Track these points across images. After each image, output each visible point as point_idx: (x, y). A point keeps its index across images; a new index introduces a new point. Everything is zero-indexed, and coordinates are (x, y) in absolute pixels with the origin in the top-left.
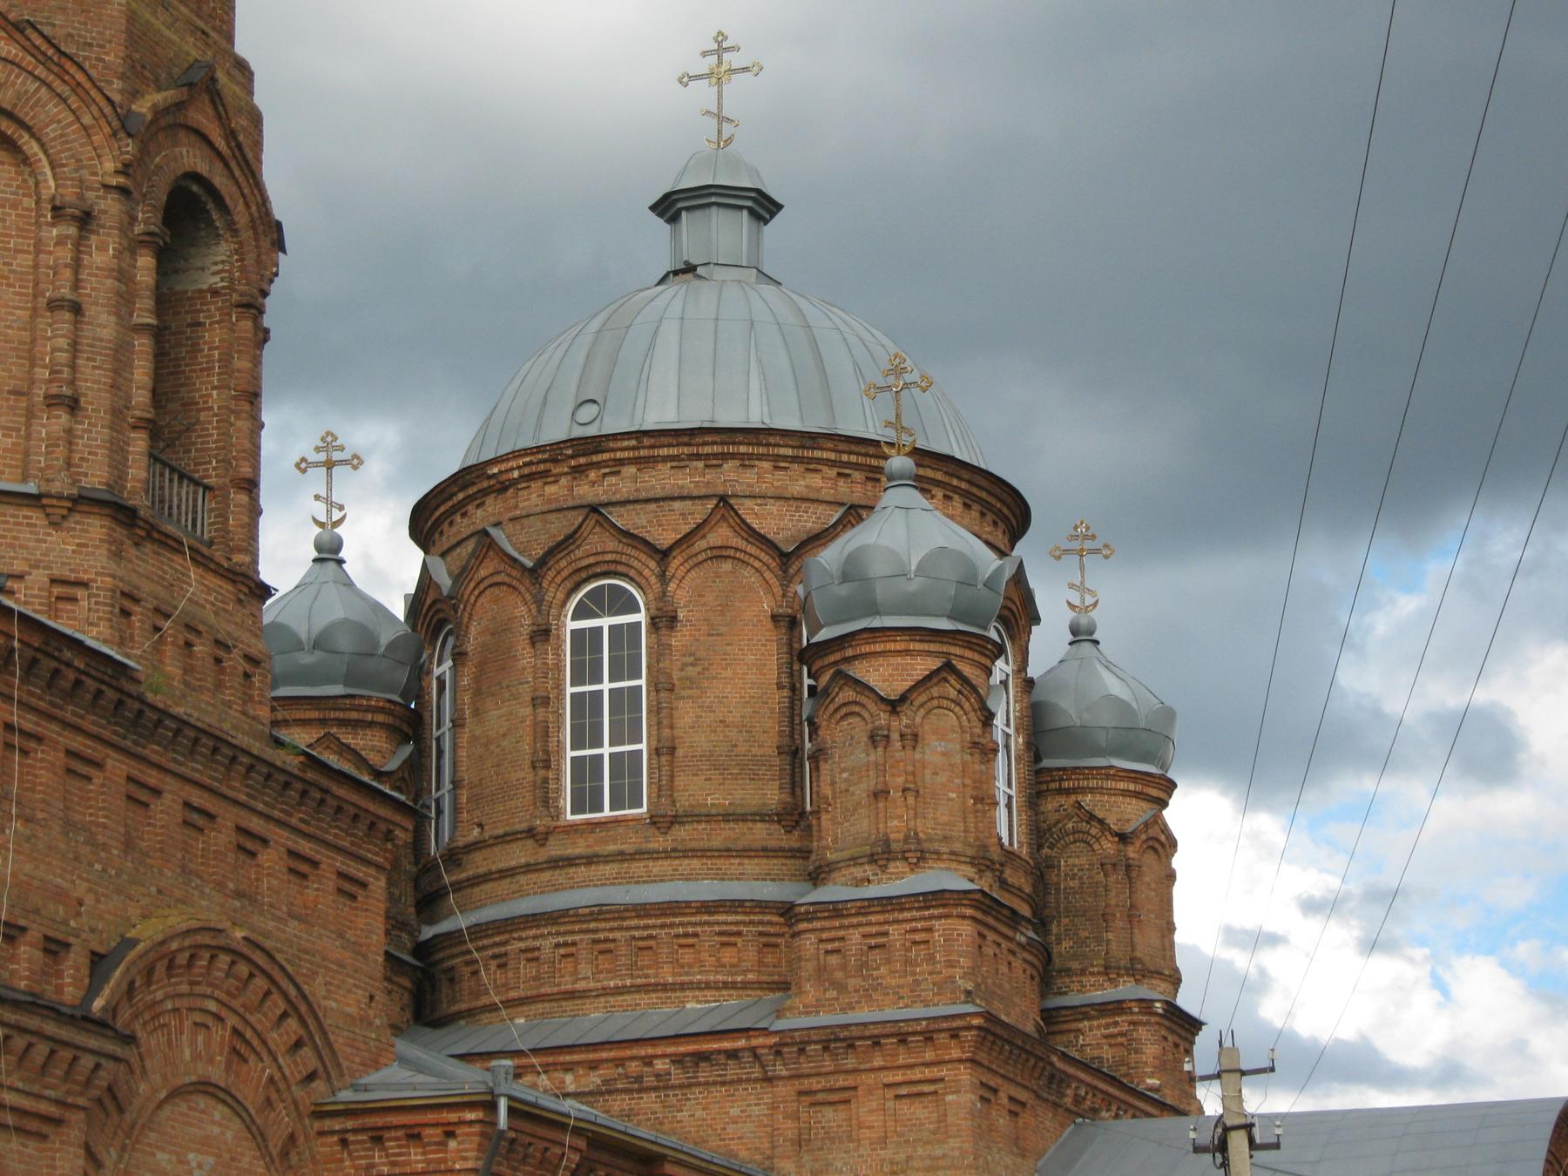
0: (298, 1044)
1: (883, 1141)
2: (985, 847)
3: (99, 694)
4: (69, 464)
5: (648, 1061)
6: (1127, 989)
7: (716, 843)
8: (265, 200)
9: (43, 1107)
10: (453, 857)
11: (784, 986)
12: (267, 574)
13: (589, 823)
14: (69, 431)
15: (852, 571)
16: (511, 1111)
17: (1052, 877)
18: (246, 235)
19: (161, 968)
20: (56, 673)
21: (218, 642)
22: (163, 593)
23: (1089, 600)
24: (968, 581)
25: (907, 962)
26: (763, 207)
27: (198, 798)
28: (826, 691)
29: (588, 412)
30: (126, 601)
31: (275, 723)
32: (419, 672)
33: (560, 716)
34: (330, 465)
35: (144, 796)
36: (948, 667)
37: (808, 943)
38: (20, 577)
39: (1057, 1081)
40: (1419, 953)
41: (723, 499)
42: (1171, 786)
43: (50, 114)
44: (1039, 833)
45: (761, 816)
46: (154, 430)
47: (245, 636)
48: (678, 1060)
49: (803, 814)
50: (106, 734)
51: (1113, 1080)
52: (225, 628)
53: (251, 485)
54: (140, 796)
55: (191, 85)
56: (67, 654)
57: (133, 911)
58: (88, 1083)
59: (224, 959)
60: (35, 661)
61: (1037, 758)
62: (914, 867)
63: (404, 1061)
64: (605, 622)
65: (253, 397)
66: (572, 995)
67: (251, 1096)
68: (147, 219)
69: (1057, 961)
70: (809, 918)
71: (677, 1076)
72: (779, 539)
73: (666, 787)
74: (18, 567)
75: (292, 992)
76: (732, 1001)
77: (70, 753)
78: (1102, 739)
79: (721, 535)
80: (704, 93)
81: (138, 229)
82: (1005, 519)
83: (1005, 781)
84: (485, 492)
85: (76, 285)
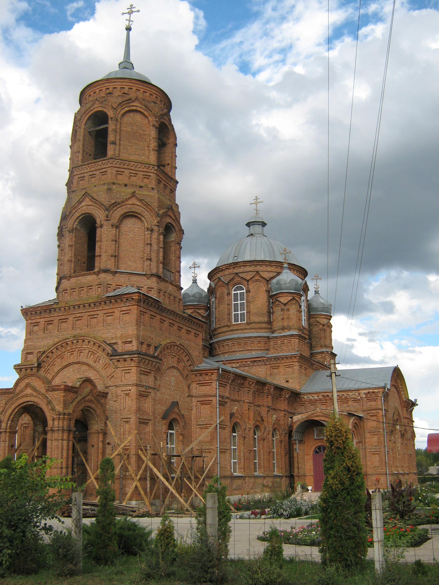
0: (188, 360)
1: (284, 375)
2: (300, 327)
3: (155, 305)
4: (150, 269)
5: (246, 362)
6: (324, 350)
7: (257, 327)
8: (181, 226)
9: (147, 371)
10: (215, 330)
11: (268, 350)
12: (182, 286)
13: (237, 324)
14: (150, 264)
15: (278, 283)
16: (222, 370)
17: (312, 332)
18: (178, 232)
19: (166, 348)
20: (148, 302)
21: (174, 297)
22: (165, 289)
23: (318, 287)
24: (297, 284)
25: (288, 346)
26: (264, 224)
27: (171, 322)
28: (274, 303)
29: (235, 258)
30: (160, 290)
31: (184, 310)
32: (209, 300)
33: (232, 307)
34: (195, 267)
35: (163, 321)
36: (294, 298)
37: (272, 343)
38: (143, 287)
39: (313, 364)
40: (378, 342)
41: (257, 272)
42: (332, 317)
43: (146, 214)
44: (310, 325)
45: (264, 323)
46: (163, 263)
47: (179, 296)
48: (251, 362)
49: (271, 322)
50: (156, 312)
51: (322, 364)
52: (175, 295)
53: (179, 272)
54: (162, 321)
55: (168, 208)
56: (150, 299)
57: (161, 340)
58: (154, 367)
59: (176, 347)
60: (145, 301)
61: (309, 312)
62: (289, 330)
63: (206, 362)
64: (239, 292)
65: (179, 258)
66: (234, 351)
67: (181, 368)
68: (162, 230)
69: (313, 345)
70: (272, 339)
71: (251, 364)
72: (266, 278)
73: (249, 318)
74: (142, 286)
75: (187, 352)
76: (260, 352)
77: (151, 315)
78: (320, 309)
79: (257, 277)
80: (254, 206)
81: (160, 232)
82: (304, 274)
83: (304, 317)
84: (219, 271)
85: (151, 241)
